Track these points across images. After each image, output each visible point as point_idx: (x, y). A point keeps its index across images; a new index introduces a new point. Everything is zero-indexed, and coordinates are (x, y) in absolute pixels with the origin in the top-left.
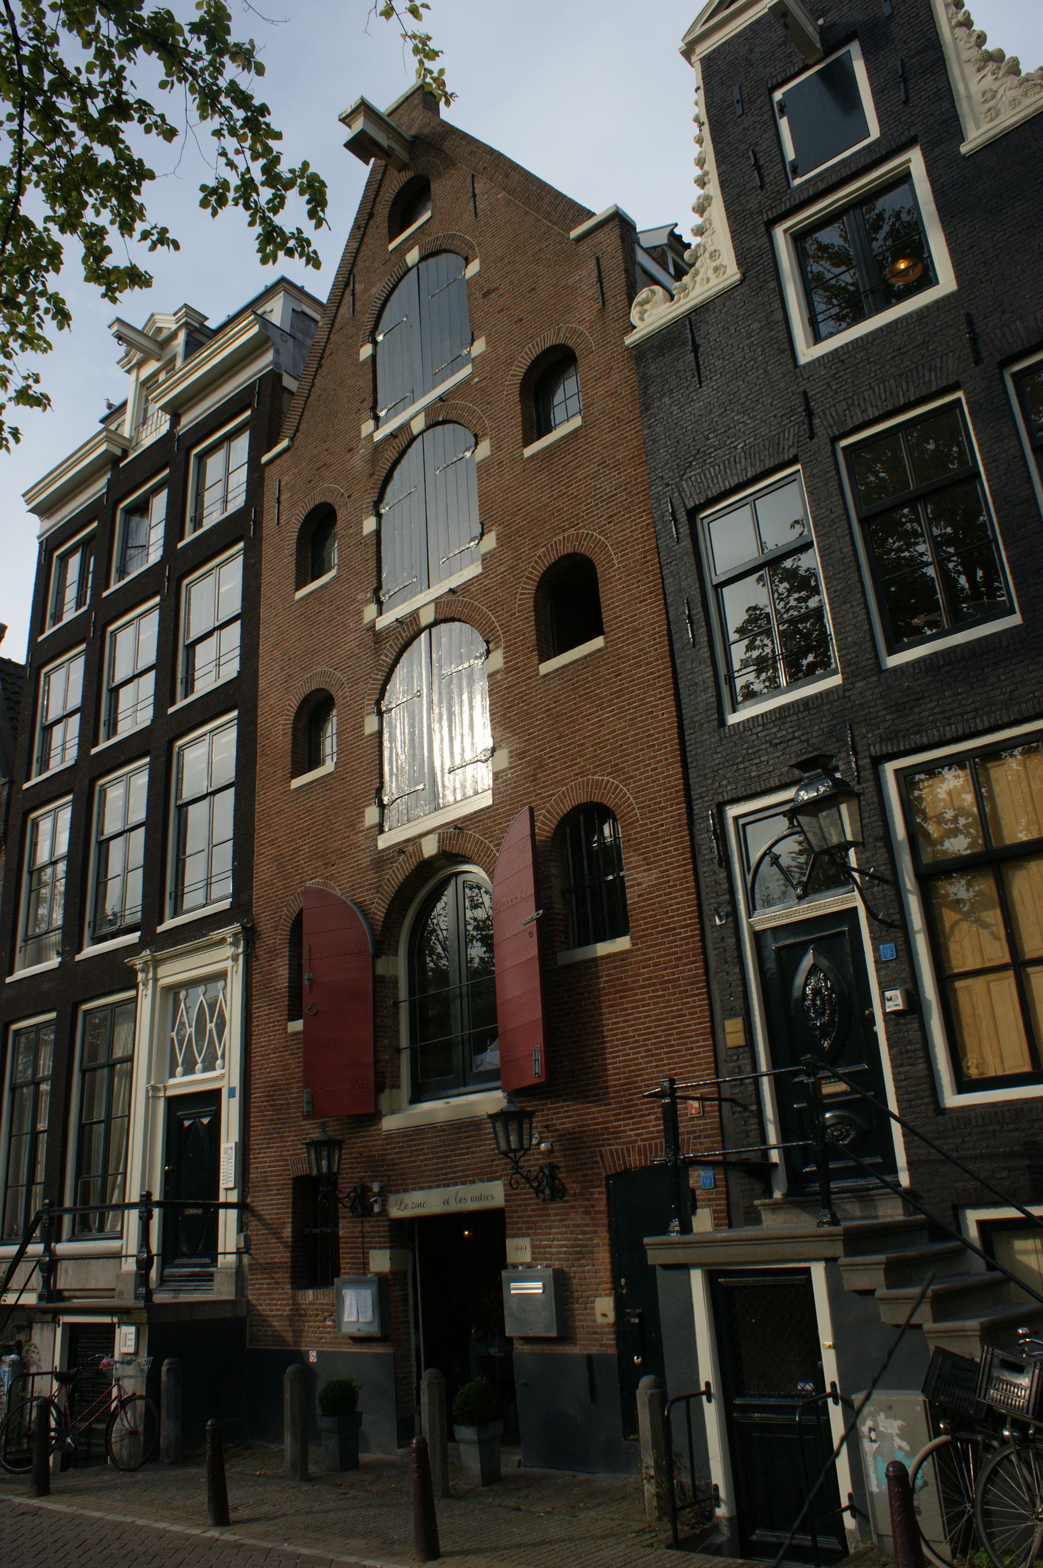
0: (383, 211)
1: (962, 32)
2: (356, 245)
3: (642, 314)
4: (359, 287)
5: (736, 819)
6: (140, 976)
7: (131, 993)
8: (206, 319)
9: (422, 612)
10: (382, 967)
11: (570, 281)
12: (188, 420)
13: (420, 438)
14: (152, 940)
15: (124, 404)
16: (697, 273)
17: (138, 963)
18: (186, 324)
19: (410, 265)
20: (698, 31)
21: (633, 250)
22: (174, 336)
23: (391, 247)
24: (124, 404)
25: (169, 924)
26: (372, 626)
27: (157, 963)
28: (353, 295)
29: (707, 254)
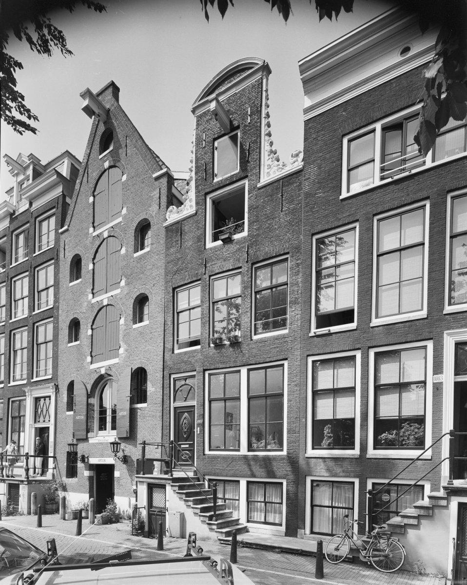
0: (97, 146)
1: (267, 138)
2: (89, 152)
3: (170, 215)
4: (90, 171)
5: (174, 378)
6: (27, 394)
7: (24, 398)
8: (40, 161)
9: (104, 301)
10: (91, 401)
11: (152, 195)
12: (37, 205)
13: (106, 240)
14: (30, 384)
15: (13, 188)
16: (185, 206)
17: (26, 390)
18: (33, 162)
19: (106, 168)
20: (197, 104)
21: (171, 188)
22: (28, 166)
23: (101, 157)
24: (13, 188)
25: (35, 379)
26: (90, 301)
27: (31, 391)
28: (88, 173)
29: (189, 199)
